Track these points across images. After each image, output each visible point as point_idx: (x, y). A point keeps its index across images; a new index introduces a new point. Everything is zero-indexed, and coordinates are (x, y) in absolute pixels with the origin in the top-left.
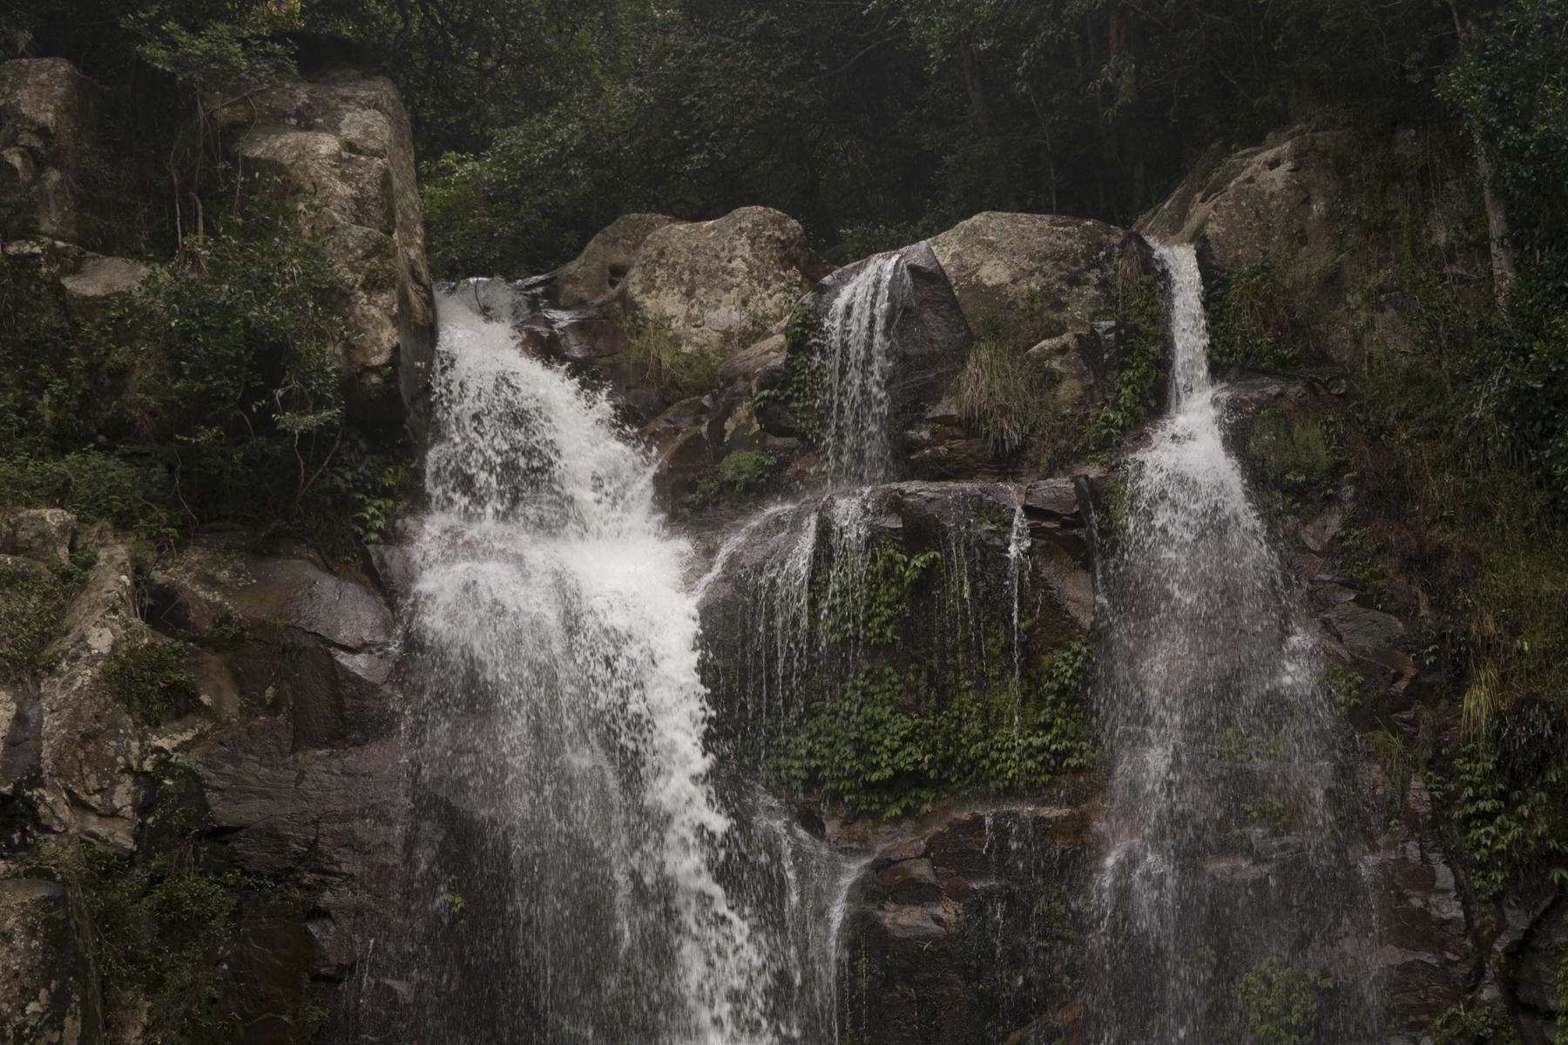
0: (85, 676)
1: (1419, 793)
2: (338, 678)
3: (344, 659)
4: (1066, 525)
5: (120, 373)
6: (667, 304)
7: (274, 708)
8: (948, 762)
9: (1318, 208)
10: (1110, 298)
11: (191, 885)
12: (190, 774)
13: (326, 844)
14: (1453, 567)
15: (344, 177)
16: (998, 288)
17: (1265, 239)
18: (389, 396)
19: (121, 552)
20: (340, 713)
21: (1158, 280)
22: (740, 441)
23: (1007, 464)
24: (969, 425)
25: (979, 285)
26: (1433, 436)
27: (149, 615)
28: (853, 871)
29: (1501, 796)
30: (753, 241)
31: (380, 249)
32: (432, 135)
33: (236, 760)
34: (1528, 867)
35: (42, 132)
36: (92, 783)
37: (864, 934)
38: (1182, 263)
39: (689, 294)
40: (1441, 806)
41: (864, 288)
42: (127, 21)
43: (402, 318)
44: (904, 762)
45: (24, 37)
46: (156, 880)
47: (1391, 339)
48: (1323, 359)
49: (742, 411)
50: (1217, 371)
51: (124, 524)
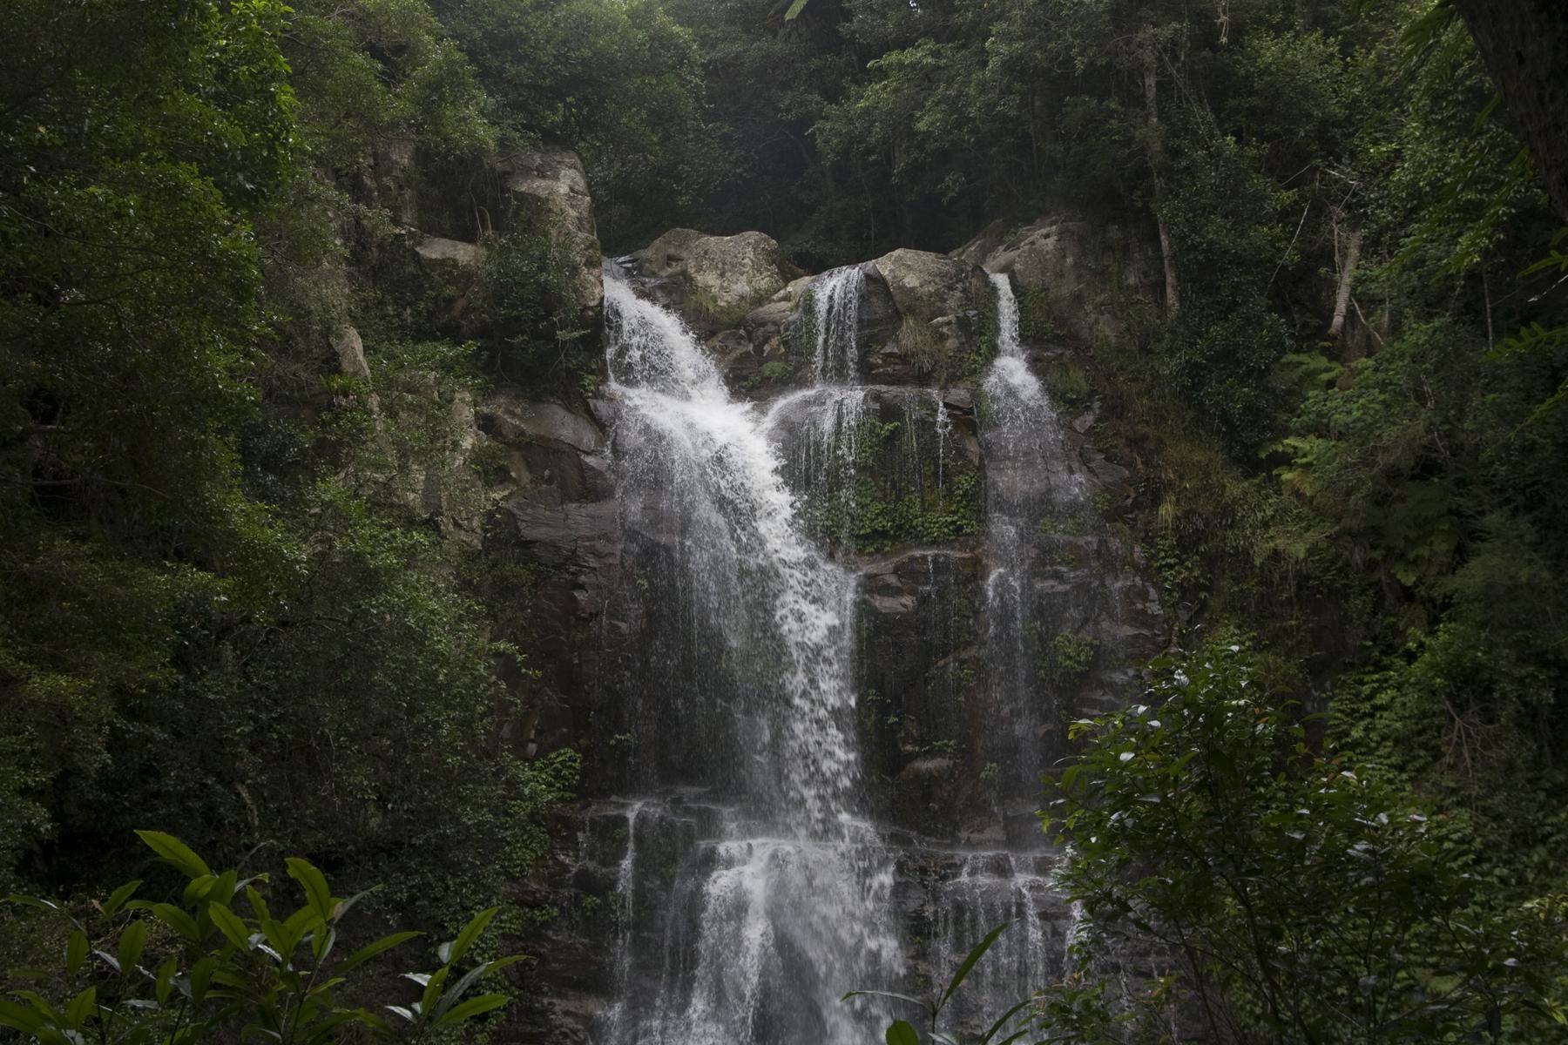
2: (582, 468)
4: (966, 413)
6: (709, 279)
7: (550, 480)
8: (900, 527)
9: (1069, 260)
10: (968, 300)
12: (509, 513)
13: (580, 552)
14: (1151, 445)
15: (572, 206)
16: (913, 289)
17: (1044, 274)
21: (993, 290)
23: (923, 379)
24: (904, 358)
25: (903, 287)
26: (1135, 380)
29: (1178, 556)
30: (755, 250)
33: (533, 507)
36: (464, 515)
38: (1002, 281)
39: (722, 275)
46: (494, 565)
49: (775, 341)
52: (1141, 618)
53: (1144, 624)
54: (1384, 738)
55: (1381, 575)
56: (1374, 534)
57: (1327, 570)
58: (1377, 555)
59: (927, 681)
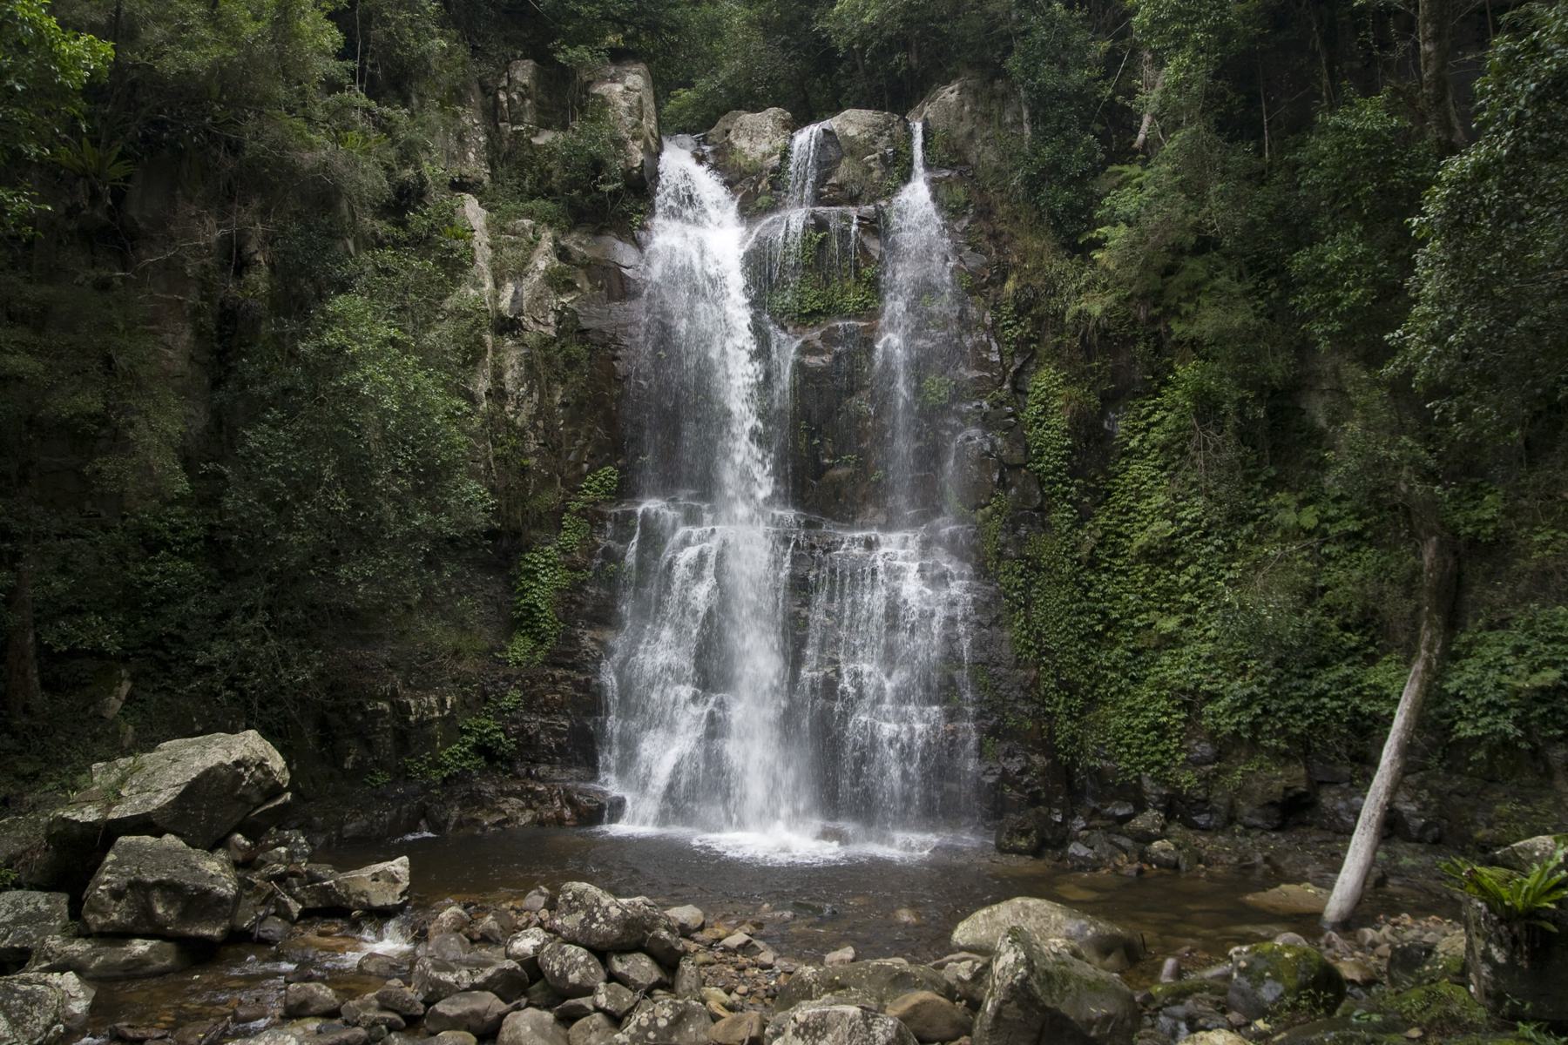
0: (537, 277)
1: (988, 319)
3: (624, 271)
5: (550, 172)
6: (742, 143)
7: (601, 288)
9: (967, 108)
11: (574, 349)
14: (1005, 238)
18: (641, 178)
19: (549, 234)
20: (619, 287)
22: (764, 193)
23: (854, 200)
24: (841, 186)
27: (560, 257)
28: (798, 343)
31: (637, 125)
32: (662, 87)
34: (1023, 344)
35: (524, 86)
37: (799, 367)
40: (995, 323)
41: (805, 138)
42: (550, 46)
43: (646, 148)
44: (814, 306)
45: (520, 53)
47: (991, 156)
48: (966, 163)
49: (764, 182)
50: (928, 167)
51: (551, 224)
52: (984, 365)
53: (986, 369)
54: (1154, 447)
55: (1161, 327)
56: (1154, 297)
57: (1121, 326)
58: (1155, 312)
59: (839, 414)
